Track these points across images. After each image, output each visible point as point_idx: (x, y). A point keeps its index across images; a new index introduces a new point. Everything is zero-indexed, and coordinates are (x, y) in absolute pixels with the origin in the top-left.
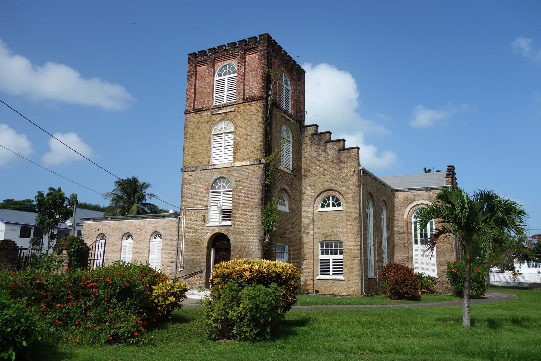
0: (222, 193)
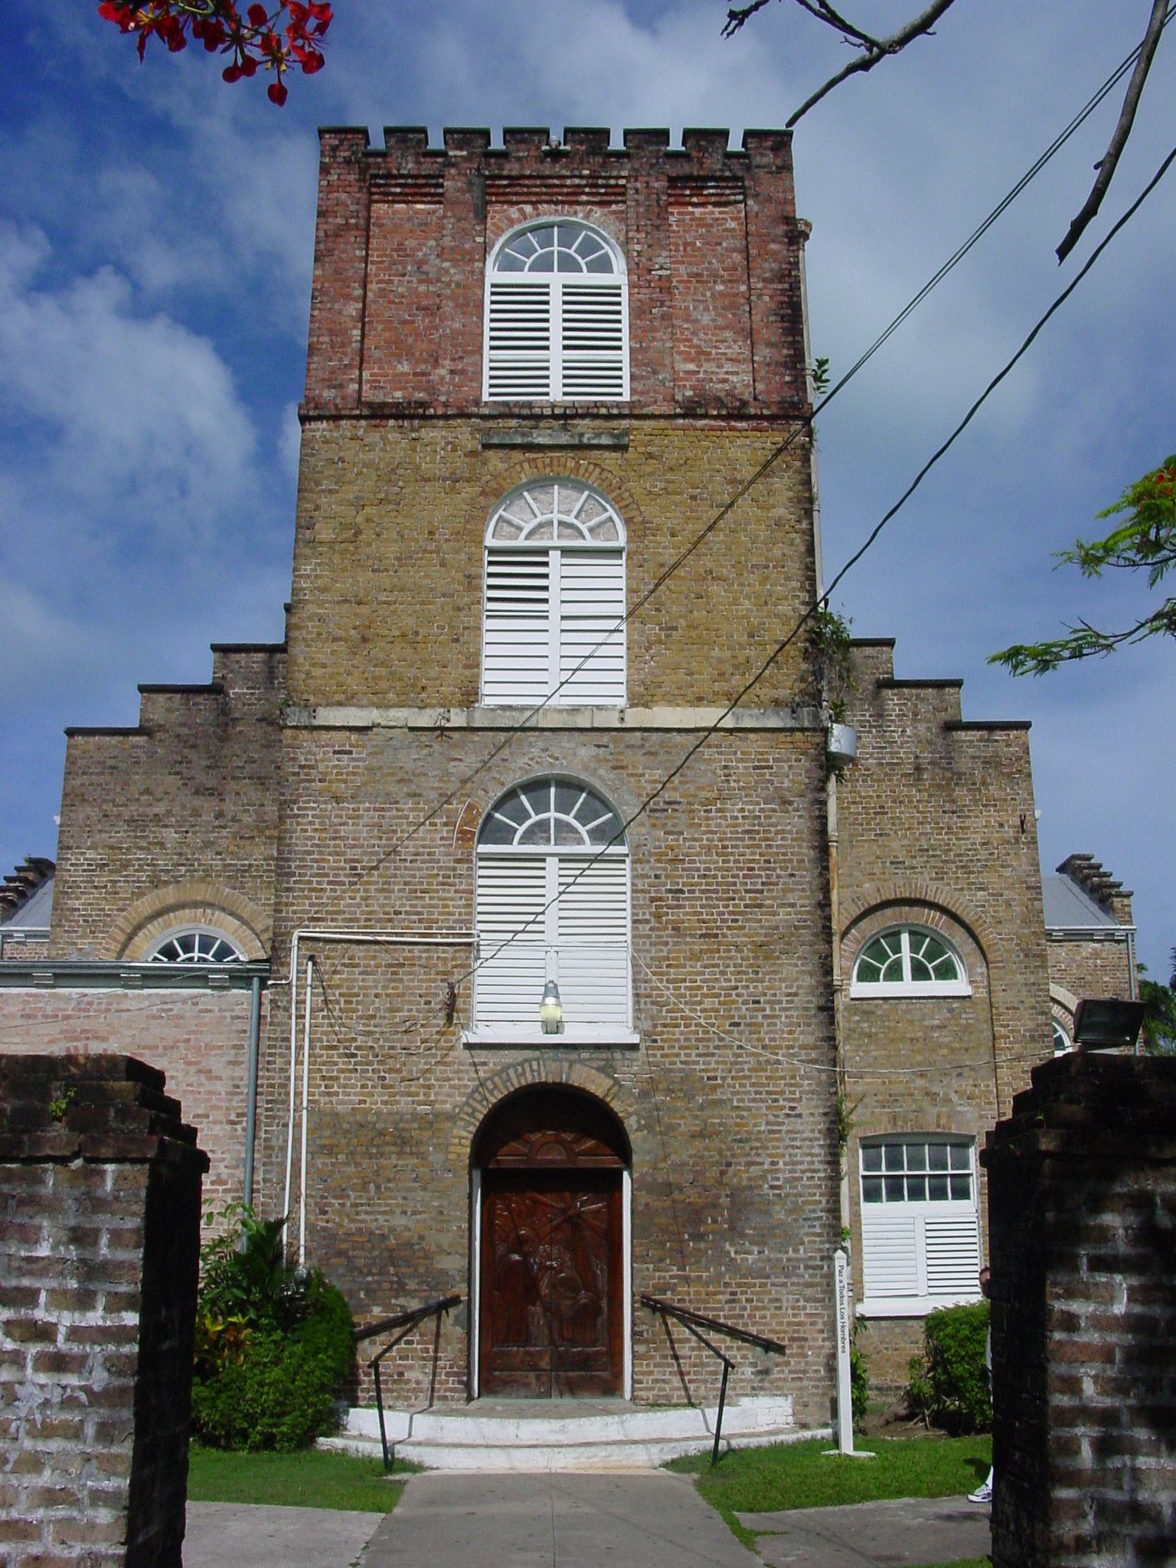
0: (552, 863)
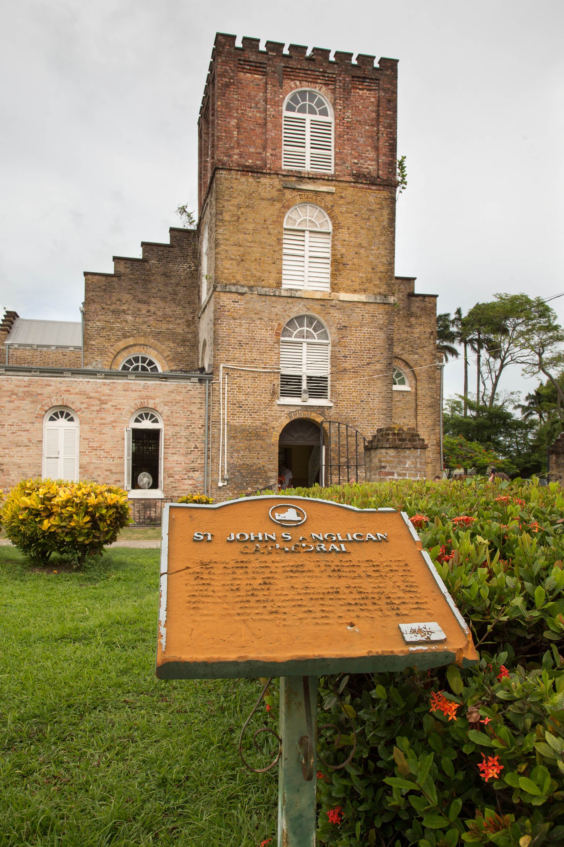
0: (305, 345)
